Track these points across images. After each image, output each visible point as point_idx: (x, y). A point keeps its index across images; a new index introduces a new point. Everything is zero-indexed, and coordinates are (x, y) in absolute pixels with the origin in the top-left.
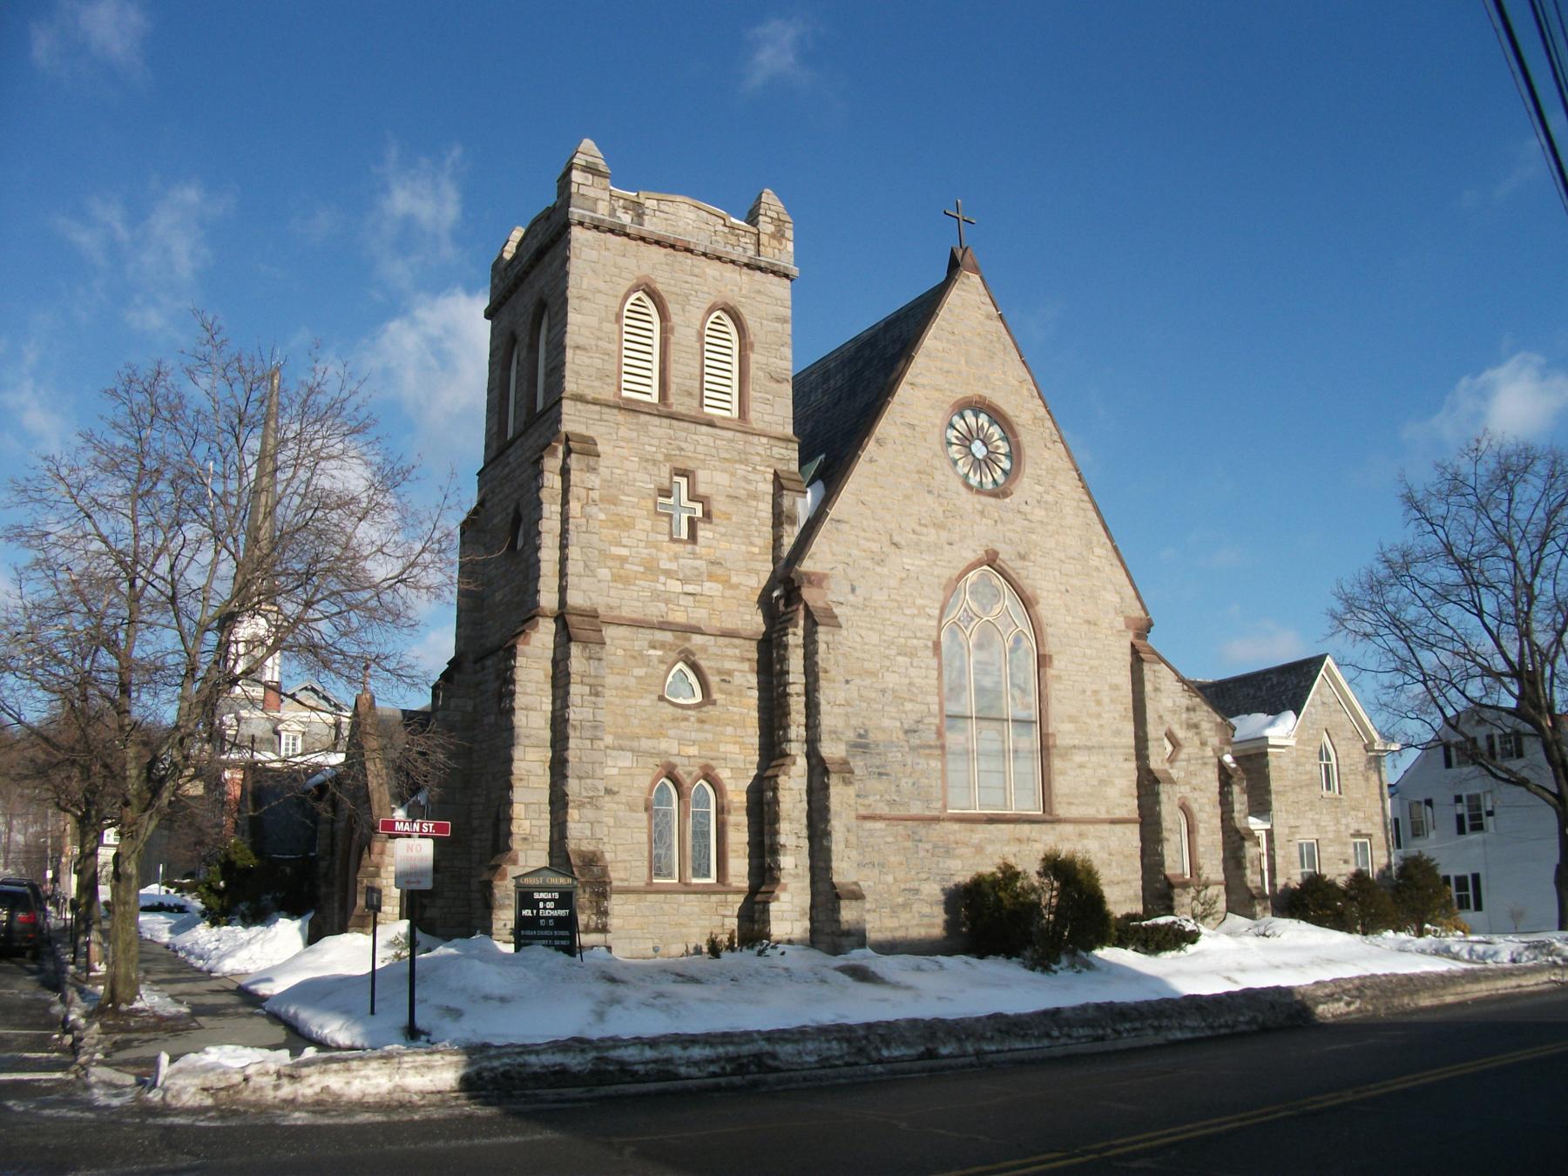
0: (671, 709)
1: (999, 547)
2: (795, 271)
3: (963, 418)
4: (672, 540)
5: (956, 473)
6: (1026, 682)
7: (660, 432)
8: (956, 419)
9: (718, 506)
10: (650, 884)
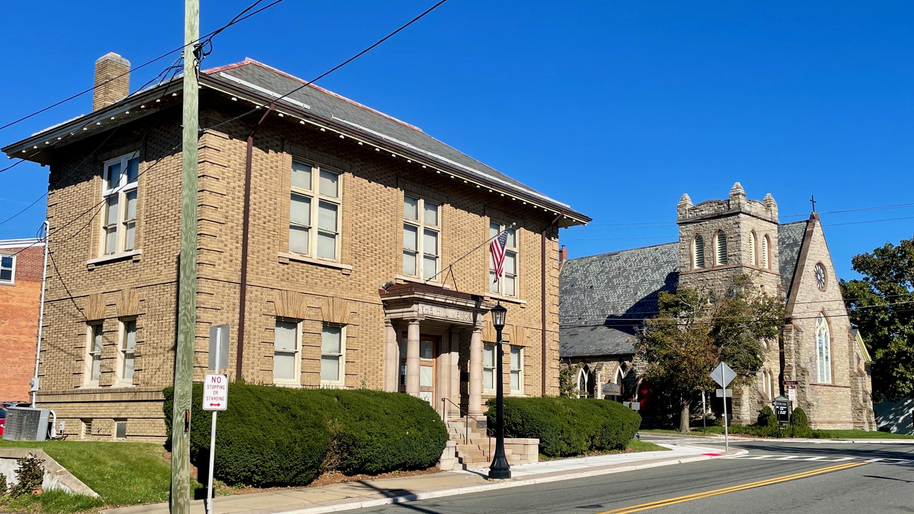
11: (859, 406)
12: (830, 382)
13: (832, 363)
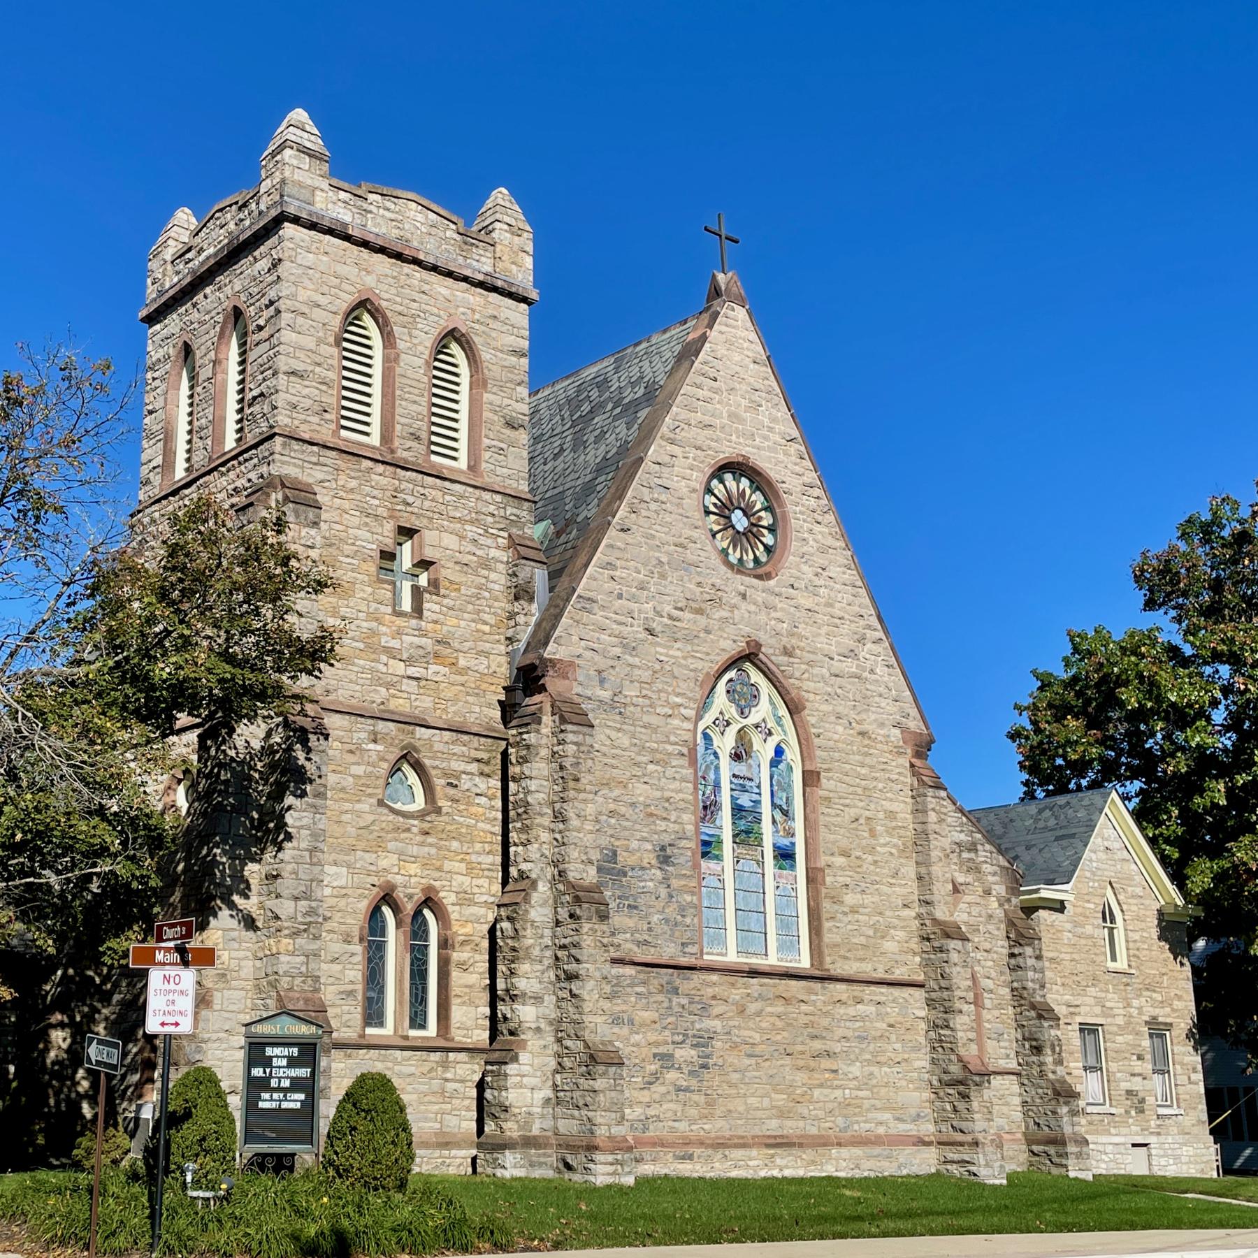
0: (391, 817)
1: (762, 637)
2: (534, 295)
3: (722, 481)
4: (398, 614)
5: (715, 547)
6: (789, 800)
7: (384, 481)
8: (715, 482)
9: (448, 572)
10: (363, 1036)
11: (955, 1069)
12: (804, 962)
13: (814, 878)
